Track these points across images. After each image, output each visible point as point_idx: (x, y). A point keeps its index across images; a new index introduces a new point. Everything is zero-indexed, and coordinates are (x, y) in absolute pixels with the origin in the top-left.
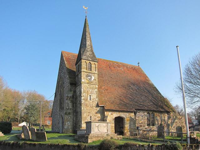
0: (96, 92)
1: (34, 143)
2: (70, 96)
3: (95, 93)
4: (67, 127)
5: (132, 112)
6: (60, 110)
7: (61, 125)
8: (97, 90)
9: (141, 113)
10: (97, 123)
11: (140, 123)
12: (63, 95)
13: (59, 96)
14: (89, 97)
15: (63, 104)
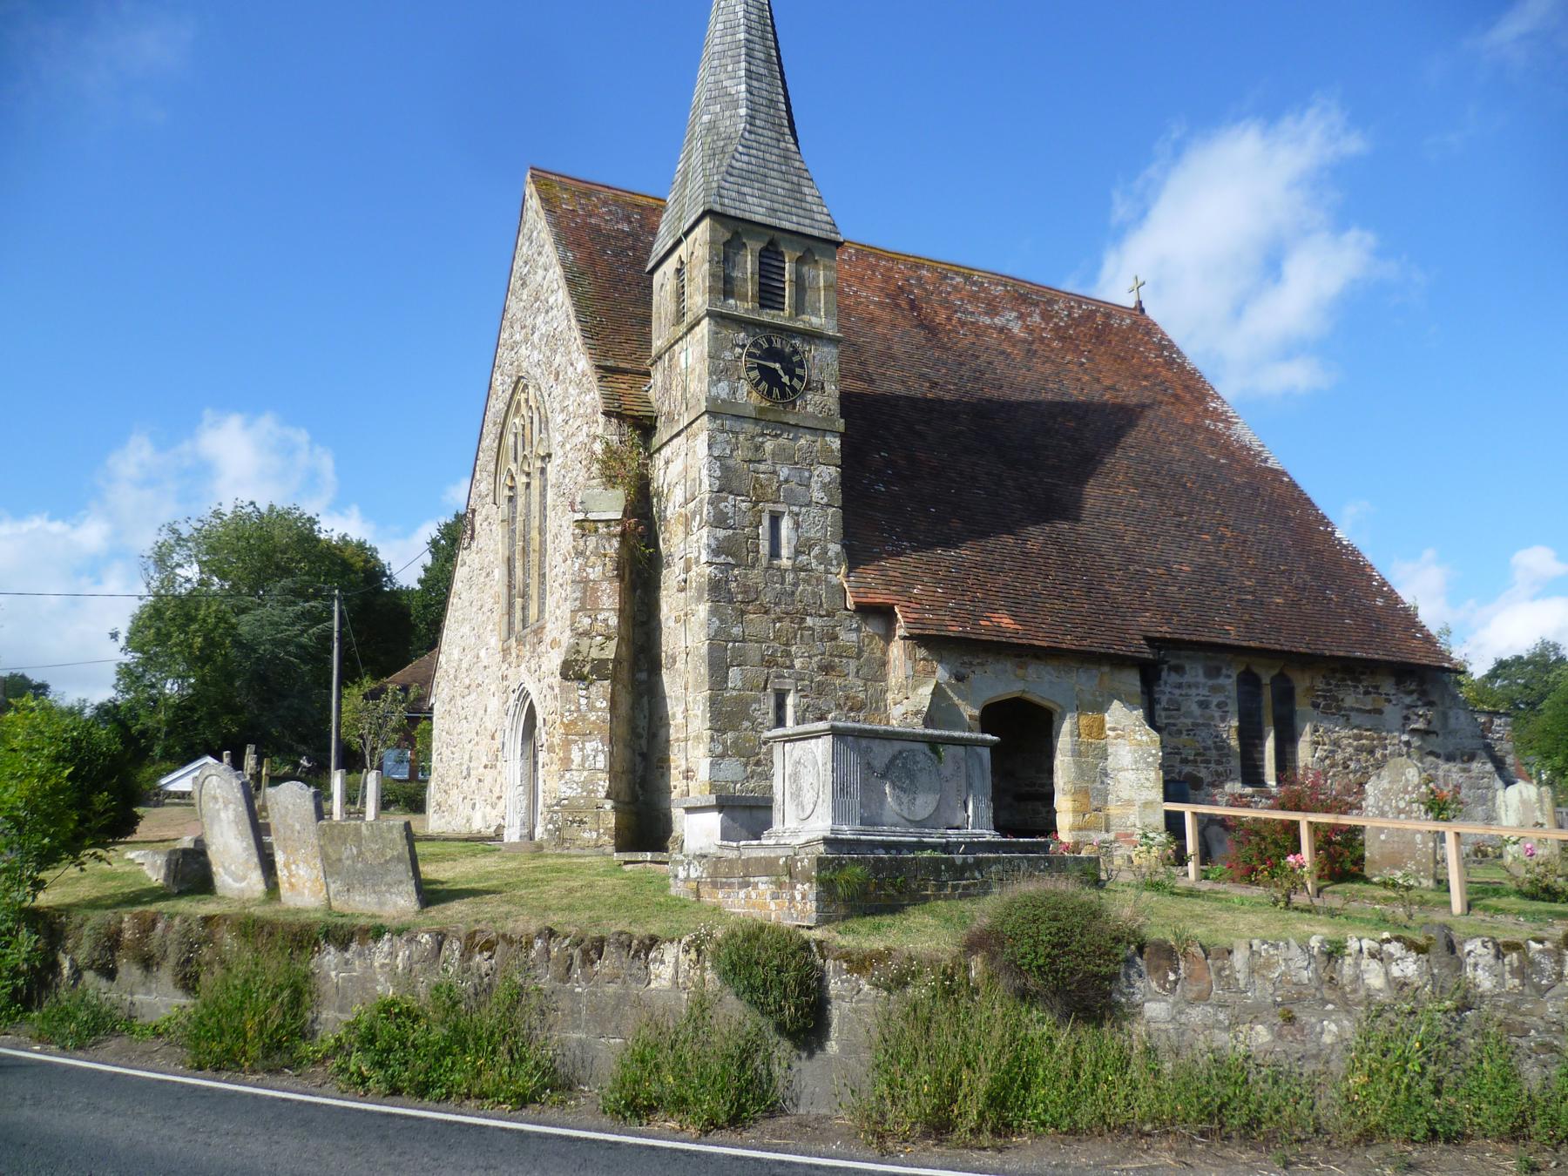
0: (824, 486)
1: (535, 597)
2: (608, 522)
3: (817, 495)
4: (584, 785)
5: (1119, 662)
6: (506, 651)
7: (513, 767)
8: (833, 469)
9: (1195, 673)
10: (877, 746)
11: (1185, 761)
12: (535, 523)
13: (499, 531)
14: (764, 530)
15: (534, 591)
